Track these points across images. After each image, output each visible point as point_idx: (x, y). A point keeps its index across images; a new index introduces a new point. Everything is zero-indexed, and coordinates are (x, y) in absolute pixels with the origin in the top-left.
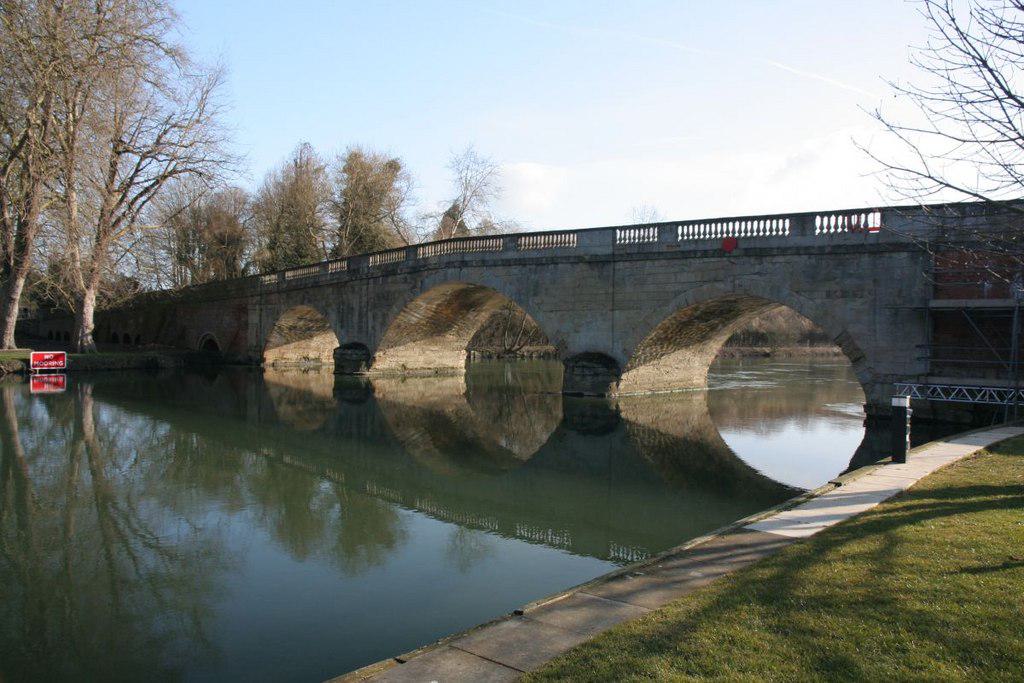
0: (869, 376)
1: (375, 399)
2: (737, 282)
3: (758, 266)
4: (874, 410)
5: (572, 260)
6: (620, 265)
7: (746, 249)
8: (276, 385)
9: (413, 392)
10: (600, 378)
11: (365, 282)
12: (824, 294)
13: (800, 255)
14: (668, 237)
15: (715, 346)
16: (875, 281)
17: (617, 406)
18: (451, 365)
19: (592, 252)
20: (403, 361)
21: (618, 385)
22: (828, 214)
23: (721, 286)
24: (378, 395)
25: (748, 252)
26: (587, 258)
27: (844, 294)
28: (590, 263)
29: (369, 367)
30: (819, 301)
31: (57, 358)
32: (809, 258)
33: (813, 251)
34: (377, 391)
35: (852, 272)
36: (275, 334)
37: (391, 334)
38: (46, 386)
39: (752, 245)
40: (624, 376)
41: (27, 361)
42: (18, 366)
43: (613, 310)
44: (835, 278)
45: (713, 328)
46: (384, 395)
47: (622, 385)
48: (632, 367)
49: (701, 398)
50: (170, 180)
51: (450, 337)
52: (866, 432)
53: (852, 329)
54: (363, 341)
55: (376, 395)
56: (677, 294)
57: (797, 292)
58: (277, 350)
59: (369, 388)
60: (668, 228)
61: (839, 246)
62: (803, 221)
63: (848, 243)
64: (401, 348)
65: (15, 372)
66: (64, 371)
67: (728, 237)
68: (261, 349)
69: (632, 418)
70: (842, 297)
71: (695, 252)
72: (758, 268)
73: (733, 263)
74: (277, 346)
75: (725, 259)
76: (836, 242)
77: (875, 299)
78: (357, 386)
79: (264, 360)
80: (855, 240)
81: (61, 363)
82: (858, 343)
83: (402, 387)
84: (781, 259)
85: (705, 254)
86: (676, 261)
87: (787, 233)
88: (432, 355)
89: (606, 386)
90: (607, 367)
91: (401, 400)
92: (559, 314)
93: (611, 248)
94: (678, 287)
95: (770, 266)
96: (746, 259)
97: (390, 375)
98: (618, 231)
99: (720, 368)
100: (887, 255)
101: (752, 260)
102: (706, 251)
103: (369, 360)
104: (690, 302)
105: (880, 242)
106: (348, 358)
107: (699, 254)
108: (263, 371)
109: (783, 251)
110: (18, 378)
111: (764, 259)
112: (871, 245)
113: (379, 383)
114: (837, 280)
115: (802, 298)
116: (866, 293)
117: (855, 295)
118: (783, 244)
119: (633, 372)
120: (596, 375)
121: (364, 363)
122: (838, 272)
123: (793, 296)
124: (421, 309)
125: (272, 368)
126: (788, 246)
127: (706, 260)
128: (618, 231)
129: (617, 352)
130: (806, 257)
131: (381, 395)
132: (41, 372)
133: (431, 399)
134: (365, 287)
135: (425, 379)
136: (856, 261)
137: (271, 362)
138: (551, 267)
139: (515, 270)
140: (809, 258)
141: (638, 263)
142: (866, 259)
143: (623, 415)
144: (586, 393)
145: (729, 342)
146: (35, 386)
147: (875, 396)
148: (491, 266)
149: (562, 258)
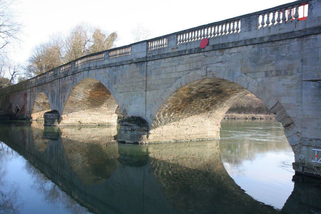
0: (297, 139)
1: (61, 138)
2: (208, 69)
3: (220, 57)
4: (301, 168)
5: (129, 63)
6: (150, 63)
7: (213, 46)
8: (37, 129)
9: (84, 135)
10: (135, 133)
11: (59, 80)
12: (264, 74)
13: (247, 45)
14: (173, 43)
15: (220, 113)
16: (302, 61)
17: (147, 150)
18: (107, 121)
19: (137, 57)
20: (79, 119)
21: (148, 137)
22: (267, 12)
23: (199, 72)
25: (215, 48)
26: (134, 60)
27: (278, 73)
28: (135, 63)
29: (59, 122)
30: (259, 80)
32: (253, 47)
33: (255, 42)
34: (63, 134)
35: (284, 55)
37: (68, 106)
39: (217, 43)
40: (151, 132)
43: (146, 91)
44: (271, 61)
45: (214, 103)
46: (67, 136)
47: (151, 137)
48: (156, 127)
49: (214, 144)
50: (219, 67)
51: (104, 108)
52: (295, 185)
53: (284, 101)
54: (57, 109)
55: (62, 137)
56: (176, 79)
57: (245, 74)
58: (38, 113)
59: (59, 134)
60: (172, 37)
61: (274, 36)
62: (249, 19)
63: (282, 32)
64: (77, 113)
67: (204, 39)
68: (30, 113)
70: (277, 75)
71: (185, 51)
72: (220, 58)
73: (206, 56)
74: (38, 111)
75: (201, 54)
76: (273, 32)
77: (302, 75)
78: (53, 133)
79: (31, 118)
80: (287, 29)
82: (288, 112)
83: (79, 132)
84: (234, 50)
85: (191, 52)
86: (176, 58)
87: (239, 31)
88: (96, 116)
89: (140, 137)
91: (76, 139)
92: (124, 93)
94: (177, 75)
95: (228, 55)
96: (213, 52)
97: (68, 126)
99: (225, 127)
100: (313, 37)
101: (217, 53)
102: (191, 50)
103: (59, 119)
104: (183, 84)
105: (307, 27)
106: (49, 118)
107: (187, 52)
108: (31, 123)
109: (236, 44)
111: (224, 51)
112: (299, 31)
113: (65, 130)
114: (273, 62)
115: (248, 78)
116: (295, 71)
117: (286, 74)
118: (236, 39)
119: (159, 129)
120: (133, 130)
121: (57, 120)
122: (274, 56)
123: (242, 77)
124: (81, 92)
125: (35, 122)
126: (240, 40)
127: (191, 55)
129: (147, 118)
130: (250, 47)
131: (65, 136)
133: (94, 139)
134: (59, 82)
135: (92, 129)
136: (287, 45)
137: (35, 119)
138: (121, 67)
139: (107, 70)
140: (253, 47)
141: (158, 61)
142: (295, 43)
145: (231, 110)
147: (302, 156)
149: (125, 62)
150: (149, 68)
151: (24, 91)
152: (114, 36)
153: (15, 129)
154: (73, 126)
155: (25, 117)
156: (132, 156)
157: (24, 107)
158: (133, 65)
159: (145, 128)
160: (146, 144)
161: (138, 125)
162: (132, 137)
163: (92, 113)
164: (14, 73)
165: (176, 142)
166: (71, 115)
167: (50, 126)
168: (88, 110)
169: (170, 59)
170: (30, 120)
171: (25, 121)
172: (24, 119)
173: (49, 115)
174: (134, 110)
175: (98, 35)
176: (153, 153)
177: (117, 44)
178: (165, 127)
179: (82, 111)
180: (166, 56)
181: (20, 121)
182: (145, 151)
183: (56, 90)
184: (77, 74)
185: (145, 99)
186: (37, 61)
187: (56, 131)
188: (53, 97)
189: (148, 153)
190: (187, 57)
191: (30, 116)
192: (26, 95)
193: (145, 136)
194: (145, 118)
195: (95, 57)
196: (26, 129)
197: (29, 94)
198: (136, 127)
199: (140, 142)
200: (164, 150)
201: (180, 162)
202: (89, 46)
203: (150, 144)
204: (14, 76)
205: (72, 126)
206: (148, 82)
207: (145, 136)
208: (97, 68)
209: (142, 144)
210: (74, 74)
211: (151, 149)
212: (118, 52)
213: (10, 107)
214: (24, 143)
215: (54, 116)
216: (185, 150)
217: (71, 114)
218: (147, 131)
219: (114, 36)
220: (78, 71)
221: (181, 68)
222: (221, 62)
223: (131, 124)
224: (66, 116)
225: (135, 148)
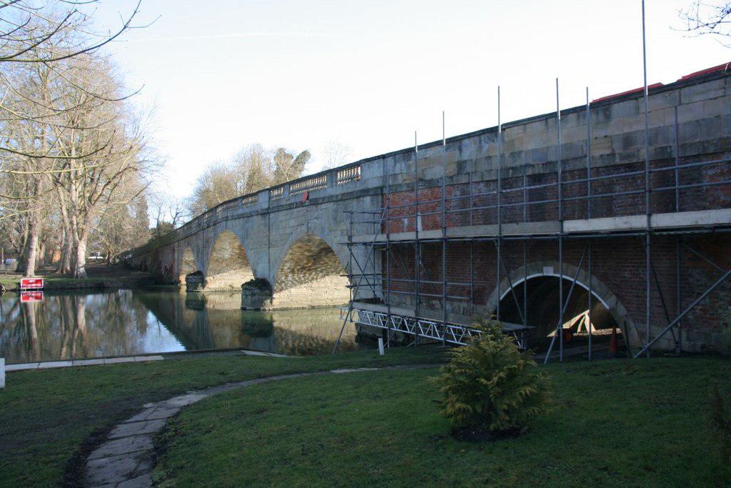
1: (206, 309)
6: (272, 215)
10: (256, 297)
17: (271, 317)
20: (230, 282)
21: (271, 302)
24: (209, 306)
29: (203, 286)
31: (37, 282)
36: (184, 265)
38: (30, 298)
40: (275, 295)
41: (19, 284)
42: (14, 286)
43: (269, 248)
46: (214, 306)
47: (275, 302)
54: (201, 270)
64: (225, 274)
65: (12, 290)
66: (43, 290)
69: (284, 325)
78: (197, 300)
81: (39, 285)
83: (230, 300)
89: (262, 302)
90: (262, 290)
93: (267, 204)
97: (216, 292)
98: (511, 171)
103: (204, 283)
110: (14, 294)
113: (211, 298)
119: (284, 294)
120: (253, 295)
121: (200, 284)
127: (299, 209)
128: (511, 171)
131: (212, 306)
132: (28, 290)
139: (241, 221)
143: (275, 324)
144: (248, 308)
146: (24, 299)
148: (236, 219)
150: (272, 221)
151: (172, 246)
152: (304, 156)
153: (164, 296)
154: (222, 292)
155: (173, 280)
156: (253, 325)
157: (172, 267)
158: (260, 216)
159: (267, 292)
160: (270, 310)
161: (260, 288)
162: (253, 303)
163: (246, 273)
164: (177, 214)
165: (313, 308)
166: (218, 276)
167: (192, 291)
168: (241, 270)
169: (285, 211)
170: (179, 285)
171: (173, 286)
172: (173, 284)
173: (191, 277)
174: (263, 271)
175: (282, 154)
176: (279, 321)
177: (311, 168)
178: (293, 290)
179: (232, 271)
180: (320, 201)
181: (168, 286)
182: (269, 319)
183: (200, 243)
184: (218, 225)
185: (267, 257)
186: (203, 193)
187: (200, 298)
188: (198, 252)
189: (272, 321)
190: (295, 210)
191: (179, 279)
192: (174, 251)
193: (269, 301)
194: (269, 280)
195: (232, 204)
196: (175, 296)
197: (176, 249)
198: (257, 291)
199: (262, 309)
200: (294, 318)
201: (315, 334)
202: (269, 176)
203: (274, 310)
204: (177, 219)
205: (220, 291)
206: (271, 237)
207: (269, 301)
208: (234, 218)
209: (264, 310)
210: (215, 225)
211: (275, 317)
212: (310, 183)
213: (159, 267)
214: (174, 317)
215: (198, 278)
216: (325, 318)
217: (219, 275)
218: (270, 296)
219: (304, 156)
220: (219, 221)
221: (292, 223)
222: (316, 218)
223: (252, 288)
224: (211, 278)
225: (257, 315)
